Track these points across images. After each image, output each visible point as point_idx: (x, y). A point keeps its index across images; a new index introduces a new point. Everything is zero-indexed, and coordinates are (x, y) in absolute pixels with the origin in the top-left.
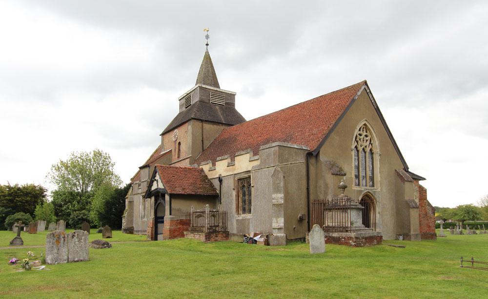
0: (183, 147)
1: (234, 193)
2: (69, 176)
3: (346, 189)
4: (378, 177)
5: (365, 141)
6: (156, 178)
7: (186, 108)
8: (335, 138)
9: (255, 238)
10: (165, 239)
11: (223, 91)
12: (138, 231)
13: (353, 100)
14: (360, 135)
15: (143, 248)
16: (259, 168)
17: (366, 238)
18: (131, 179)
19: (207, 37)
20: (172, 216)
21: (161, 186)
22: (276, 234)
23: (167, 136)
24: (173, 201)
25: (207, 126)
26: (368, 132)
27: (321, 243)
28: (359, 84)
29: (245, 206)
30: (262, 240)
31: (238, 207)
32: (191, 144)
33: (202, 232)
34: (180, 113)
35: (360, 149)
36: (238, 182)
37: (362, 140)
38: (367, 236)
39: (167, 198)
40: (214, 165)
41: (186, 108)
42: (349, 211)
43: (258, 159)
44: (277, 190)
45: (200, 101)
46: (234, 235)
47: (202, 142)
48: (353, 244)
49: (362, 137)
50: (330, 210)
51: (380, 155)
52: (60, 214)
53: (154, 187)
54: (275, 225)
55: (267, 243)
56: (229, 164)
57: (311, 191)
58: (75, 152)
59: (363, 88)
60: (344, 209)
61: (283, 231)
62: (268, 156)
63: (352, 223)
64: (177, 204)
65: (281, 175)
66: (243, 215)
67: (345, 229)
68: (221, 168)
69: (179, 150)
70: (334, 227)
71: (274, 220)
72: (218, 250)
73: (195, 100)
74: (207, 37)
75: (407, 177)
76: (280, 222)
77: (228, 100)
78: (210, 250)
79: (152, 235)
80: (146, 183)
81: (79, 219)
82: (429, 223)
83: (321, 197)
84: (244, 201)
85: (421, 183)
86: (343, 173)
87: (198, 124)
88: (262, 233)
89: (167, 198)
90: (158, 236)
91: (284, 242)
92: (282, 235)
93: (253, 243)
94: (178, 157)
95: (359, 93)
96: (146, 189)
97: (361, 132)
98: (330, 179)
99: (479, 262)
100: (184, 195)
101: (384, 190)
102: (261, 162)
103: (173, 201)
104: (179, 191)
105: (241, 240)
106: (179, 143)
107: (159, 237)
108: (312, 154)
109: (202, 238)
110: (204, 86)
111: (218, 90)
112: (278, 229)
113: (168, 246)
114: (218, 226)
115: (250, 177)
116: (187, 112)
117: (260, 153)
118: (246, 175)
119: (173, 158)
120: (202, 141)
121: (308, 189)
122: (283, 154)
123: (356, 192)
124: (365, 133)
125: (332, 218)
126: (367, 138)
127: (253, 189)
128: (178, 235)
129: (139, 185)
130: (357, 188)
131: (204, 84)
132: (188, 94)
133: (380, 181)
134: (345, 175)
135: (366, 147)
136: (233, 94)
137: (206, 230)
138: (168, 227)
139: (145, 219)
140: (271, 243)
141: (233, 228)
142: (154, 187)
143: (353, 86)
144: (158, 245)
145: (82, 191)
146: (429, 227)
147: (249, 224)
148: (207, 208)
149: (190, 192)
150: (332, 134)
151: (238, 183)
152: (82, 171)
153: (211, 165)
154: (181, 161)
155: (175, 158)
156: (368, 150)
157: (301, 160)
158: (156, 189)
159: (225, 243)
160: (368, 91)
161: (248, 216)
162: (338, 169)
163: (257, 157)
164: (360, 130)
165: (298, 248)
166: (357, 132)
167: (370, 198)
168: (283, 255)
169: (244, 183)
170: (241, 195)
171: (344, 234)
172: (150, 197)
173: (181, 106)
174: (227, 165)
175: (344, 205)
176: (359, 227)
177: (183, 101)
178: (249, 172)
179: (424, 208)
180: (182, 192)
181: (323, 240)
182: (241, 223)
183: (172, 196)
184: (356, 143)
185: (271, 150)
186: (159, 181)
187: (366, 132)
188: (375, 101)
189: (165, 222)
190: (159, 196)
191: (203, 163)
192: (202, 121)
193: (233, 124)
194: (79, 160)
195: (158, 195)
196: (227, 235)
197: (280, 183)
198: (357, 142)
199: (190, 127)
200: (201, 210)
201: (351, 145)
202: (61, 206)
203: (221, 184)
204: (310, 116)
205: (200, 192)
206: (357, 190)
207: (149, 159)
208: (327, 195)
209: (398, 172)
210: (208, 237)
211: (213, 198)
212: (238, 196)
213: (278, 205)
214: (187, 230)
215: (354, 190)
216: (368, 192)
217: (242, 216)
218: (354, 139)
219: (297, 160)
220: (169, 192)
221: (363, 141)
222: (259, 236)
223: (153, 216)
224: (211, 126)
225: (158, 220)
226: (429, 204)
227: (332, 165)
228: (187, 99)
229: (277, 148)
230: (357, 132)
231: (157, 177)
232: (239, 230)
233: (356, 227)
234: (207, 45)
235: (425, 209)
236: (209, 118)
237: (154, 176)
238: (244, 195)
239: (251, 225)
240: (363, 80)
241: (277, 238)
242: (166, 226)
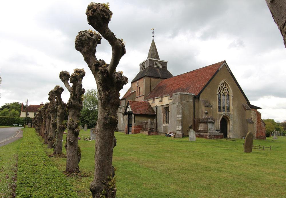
0: (141, 89)
1: (162, 114)
2: (86, 102)
3: (208, 114)
4: (231, 108)
5: (224, 90)
6: (128, 107)
7: (143, 69)
8: (208, 89)
9: (170, 135)
10: (132, 134)
11: (161, 61)
12: (120, 131)
13: (218, 71)
15: (123, 136)
16: (172, 104)
17: (214, 136)
18: (103, 60)
19: (153, 33)
20: (135, 124)
21: (130, 110)
22: (178, 133)
23: (134, 84)
25: (153, 79)
26: (226, 85)
27: (194, 137)
28: (222, 62)
29: (167, 120)
30: (173, 135)
32: (145, 89)
33: (147, 131)
34: (140, 72)
35: (222, 94)
36: (164, 109)
37: (223, 90)
38: (215, 135)
39: (133, 115)
40: (154, 101)
41: (143, 69)
42: (208, 124)
43: (172, 99)
44: (179, 114)
45: (149, 67)
46: (162, 133)
47: (150, 87)
48: (208, 138)
49: (223, 88)
50: (201, 123)
51: (233, 97)
52: (83, 121)
53: (127, 111)
54: (177, 129)
55: (175, 136)
56: (160, 100)
57: (196, 114)
58: (89, 89)
59: (223, 64)
60: (206, 123)
61: (181, 131)
62: (176, 98)
63: (209, 129)
64: (137, 119)
65: (181, 107)
66: (166, 124)
67: (206, 132)
68: (157, 103)
69: (140, 91)
70: (202, 131)
71: (177, 127)
72: (152, 138)
73: (147, 66)
74: (153, 33)
75: (247, 107)
76: (180, 128)
77: (164, 65)
78: (149, 138)
79: (127, 132)
80: (124, 107)
81: (93, 124)
82: (262, 131)
83: (200, 117)
84: (166, 118)
85: (258, 110)
86: (211, 106)
87: (149, 79)
88: (173, 132)
89: (133, 115)
91: (181, 137)
92: (181, 133)
93: (169, 137)
94: (139, 95)
95: (221, 67)
96: (124, 111)
97: (222, 86)
98: (204, 110)
99: (255, 146)
101: (235, 114)
102: (173, 101)
104: (138, 113)
105: (165, 135)
106: (140, 88)
107: (130, 133)
108: (196, 97)
109: (147, 133)
110: (151, 59)
111: (158, 60)
112: (179, 131)
113: (133, 136)
114: (154, 128)
115: (169, 107)
116: (144, 72)
117: (173, 96)
118: (167, 106)
119: (137, 95)
120: (150, 87)
121: (194, 113)
122: (182, 98)
123: (219, 115)
124: (225, 86)
125: (201, 127)
126: (226, 89)
127: (170, 113)
128: (138, 132)
129: (121, 108)
130: (220, 113)
131: (151, 58)
132: (144, 63)
133: (233, 110)
134: (212, 107)
135: (225, 93)
136: (166, 62)
137: (148, 130)
138: (134, 129)
139: (124, 125)
140: (176, 137)
141: (161, 129)
142: (127, 111)
143: (219, 63)
144: (129, 136)
145: (93, 109)
146: (262, 133)
147: (168, 128)
148: (149, 120)
149: (143, 113)
150: (206, 88)
152: (93, 100)
153: (153, 100)
154: (140, 97)
155: (137, 95)
156: (226, 94)
157: (191, 100)
158: (128, 111)
159: (157, 136)
160: (226, 65)
161: (168, 125)
162: (208, 104)
163: (171, 98)
164: (222, 85)
165: (185, 139)
166: (220, 86)
168: (177, 141)
169: (166, 109)
170: (165, 115)
171: (205, 134)
172: (126, 115)
173: (141, 68)
174: (159, 101)
175: (206, 121)
176: (213, 131)
177: (142, 66)
178: (168, 105)
179: (259, 123)
180: (139, 113)
181: (195, 136)
182: (164, 127)
183: (135, 115)
184: (219, 91)
185: (177, 95)
186: (130, 108)
187: (225, 85)
189: (132, 126)
190: (130, 114)
191: (149, 99)
192: (150, 77)
193: (166, 78)
194: (91, 93)
195: (129, 114)
196: (157, 132)
197: (180, 111)
198: (220, 91)
199: (144, 80)
200: (147, 122)
201: (216, 92)
202: (83, 117)
203: (157, 110)
204: (199, 78)
205: (147, 113)
206: (220, 114)
207: (125, 94)
208: (203, 116)
209: (243, 105)
210: (149, 133)
211: (153, 116)
212: (164, 115)
213: (179, 120)
214: (141, 130)
215: (218, 114)
216: (226, 115)
217: (166, 125)
218: (218, 89)
219: (188, 100)
220: (134, 113)
221: (224, 90)
222: (172, 134)
223: (127, 124)
224: (155, 79)
225: (130, 125)
227: (205, 102)
228: (143, 65)
229: (179, 95)
230: (220, 86)
231: (129, 106)
232: (164, 131)
233: (211, 131)
234: (153, 37)
235: (260, 124)
236: (154, 75)
237: (128, 106)
238: (166, 115)
239: (169, 129)
240: (222, 60)
241: (178, 134)
242: (133, 128)
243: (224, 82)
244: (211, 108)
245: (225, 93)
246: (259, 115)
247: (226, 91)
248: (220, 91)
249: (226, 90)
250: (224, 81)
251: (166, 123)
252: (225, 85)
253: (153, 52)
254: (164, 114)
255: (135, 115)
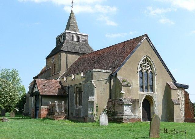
14: (144, 63)
23: (49, 59)
24: (43, 98)
25: (70, 56)
31: (77, 102)
35: (144, 71)
39: (40, 97)
53: (34, 91)
89: (40, 97)
90: (174, 105)
94: (54, 72)
97: (144, 62)
100: (48, 95)
102: (86, 79)
103: (43, 98)
106: (55, 64)
127: (83, 93)
130: (142, 93)
134: (130, 86)
142: (34, 91)
151: (77, 90)
156: (149, 72)
161: (81, 107)
164: (143, 61)
167: (149, 100)
170: (78, 96)
184: (141, 68)
188: (154, 46)
198: (142, 68)
215: (55, 102)
216: (148, 95)
218: (139, 66)
221: (146, 67)
226: (191, 102)
234: (72, 7)
238: (79, 96)
243: (146, 58)
244: (131, 88)
245: (148, 70)
246: (187, 95)
247: (149, 67)
248: (142, 68)
249: (148, 67)
250: (146, 57)
251: (79, 106)
252: (148, 62)
253: (71, 23)
254: (77, 94)
255: (42, 96)
